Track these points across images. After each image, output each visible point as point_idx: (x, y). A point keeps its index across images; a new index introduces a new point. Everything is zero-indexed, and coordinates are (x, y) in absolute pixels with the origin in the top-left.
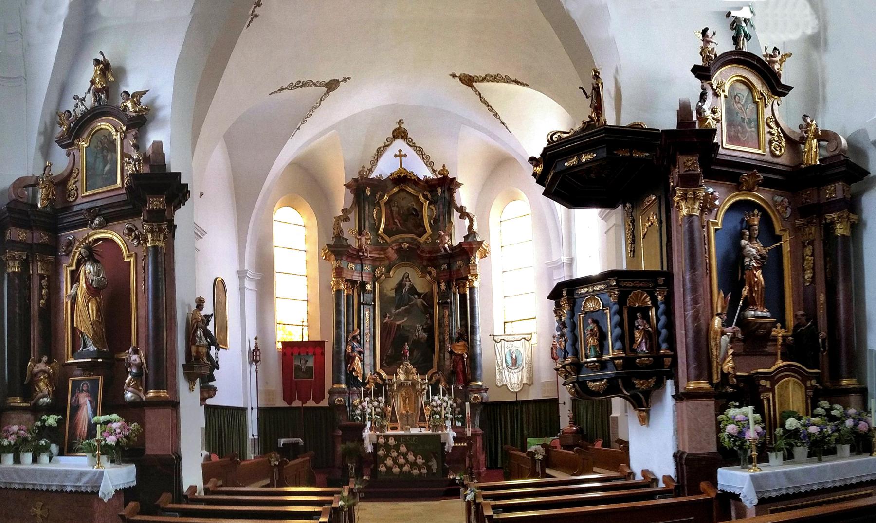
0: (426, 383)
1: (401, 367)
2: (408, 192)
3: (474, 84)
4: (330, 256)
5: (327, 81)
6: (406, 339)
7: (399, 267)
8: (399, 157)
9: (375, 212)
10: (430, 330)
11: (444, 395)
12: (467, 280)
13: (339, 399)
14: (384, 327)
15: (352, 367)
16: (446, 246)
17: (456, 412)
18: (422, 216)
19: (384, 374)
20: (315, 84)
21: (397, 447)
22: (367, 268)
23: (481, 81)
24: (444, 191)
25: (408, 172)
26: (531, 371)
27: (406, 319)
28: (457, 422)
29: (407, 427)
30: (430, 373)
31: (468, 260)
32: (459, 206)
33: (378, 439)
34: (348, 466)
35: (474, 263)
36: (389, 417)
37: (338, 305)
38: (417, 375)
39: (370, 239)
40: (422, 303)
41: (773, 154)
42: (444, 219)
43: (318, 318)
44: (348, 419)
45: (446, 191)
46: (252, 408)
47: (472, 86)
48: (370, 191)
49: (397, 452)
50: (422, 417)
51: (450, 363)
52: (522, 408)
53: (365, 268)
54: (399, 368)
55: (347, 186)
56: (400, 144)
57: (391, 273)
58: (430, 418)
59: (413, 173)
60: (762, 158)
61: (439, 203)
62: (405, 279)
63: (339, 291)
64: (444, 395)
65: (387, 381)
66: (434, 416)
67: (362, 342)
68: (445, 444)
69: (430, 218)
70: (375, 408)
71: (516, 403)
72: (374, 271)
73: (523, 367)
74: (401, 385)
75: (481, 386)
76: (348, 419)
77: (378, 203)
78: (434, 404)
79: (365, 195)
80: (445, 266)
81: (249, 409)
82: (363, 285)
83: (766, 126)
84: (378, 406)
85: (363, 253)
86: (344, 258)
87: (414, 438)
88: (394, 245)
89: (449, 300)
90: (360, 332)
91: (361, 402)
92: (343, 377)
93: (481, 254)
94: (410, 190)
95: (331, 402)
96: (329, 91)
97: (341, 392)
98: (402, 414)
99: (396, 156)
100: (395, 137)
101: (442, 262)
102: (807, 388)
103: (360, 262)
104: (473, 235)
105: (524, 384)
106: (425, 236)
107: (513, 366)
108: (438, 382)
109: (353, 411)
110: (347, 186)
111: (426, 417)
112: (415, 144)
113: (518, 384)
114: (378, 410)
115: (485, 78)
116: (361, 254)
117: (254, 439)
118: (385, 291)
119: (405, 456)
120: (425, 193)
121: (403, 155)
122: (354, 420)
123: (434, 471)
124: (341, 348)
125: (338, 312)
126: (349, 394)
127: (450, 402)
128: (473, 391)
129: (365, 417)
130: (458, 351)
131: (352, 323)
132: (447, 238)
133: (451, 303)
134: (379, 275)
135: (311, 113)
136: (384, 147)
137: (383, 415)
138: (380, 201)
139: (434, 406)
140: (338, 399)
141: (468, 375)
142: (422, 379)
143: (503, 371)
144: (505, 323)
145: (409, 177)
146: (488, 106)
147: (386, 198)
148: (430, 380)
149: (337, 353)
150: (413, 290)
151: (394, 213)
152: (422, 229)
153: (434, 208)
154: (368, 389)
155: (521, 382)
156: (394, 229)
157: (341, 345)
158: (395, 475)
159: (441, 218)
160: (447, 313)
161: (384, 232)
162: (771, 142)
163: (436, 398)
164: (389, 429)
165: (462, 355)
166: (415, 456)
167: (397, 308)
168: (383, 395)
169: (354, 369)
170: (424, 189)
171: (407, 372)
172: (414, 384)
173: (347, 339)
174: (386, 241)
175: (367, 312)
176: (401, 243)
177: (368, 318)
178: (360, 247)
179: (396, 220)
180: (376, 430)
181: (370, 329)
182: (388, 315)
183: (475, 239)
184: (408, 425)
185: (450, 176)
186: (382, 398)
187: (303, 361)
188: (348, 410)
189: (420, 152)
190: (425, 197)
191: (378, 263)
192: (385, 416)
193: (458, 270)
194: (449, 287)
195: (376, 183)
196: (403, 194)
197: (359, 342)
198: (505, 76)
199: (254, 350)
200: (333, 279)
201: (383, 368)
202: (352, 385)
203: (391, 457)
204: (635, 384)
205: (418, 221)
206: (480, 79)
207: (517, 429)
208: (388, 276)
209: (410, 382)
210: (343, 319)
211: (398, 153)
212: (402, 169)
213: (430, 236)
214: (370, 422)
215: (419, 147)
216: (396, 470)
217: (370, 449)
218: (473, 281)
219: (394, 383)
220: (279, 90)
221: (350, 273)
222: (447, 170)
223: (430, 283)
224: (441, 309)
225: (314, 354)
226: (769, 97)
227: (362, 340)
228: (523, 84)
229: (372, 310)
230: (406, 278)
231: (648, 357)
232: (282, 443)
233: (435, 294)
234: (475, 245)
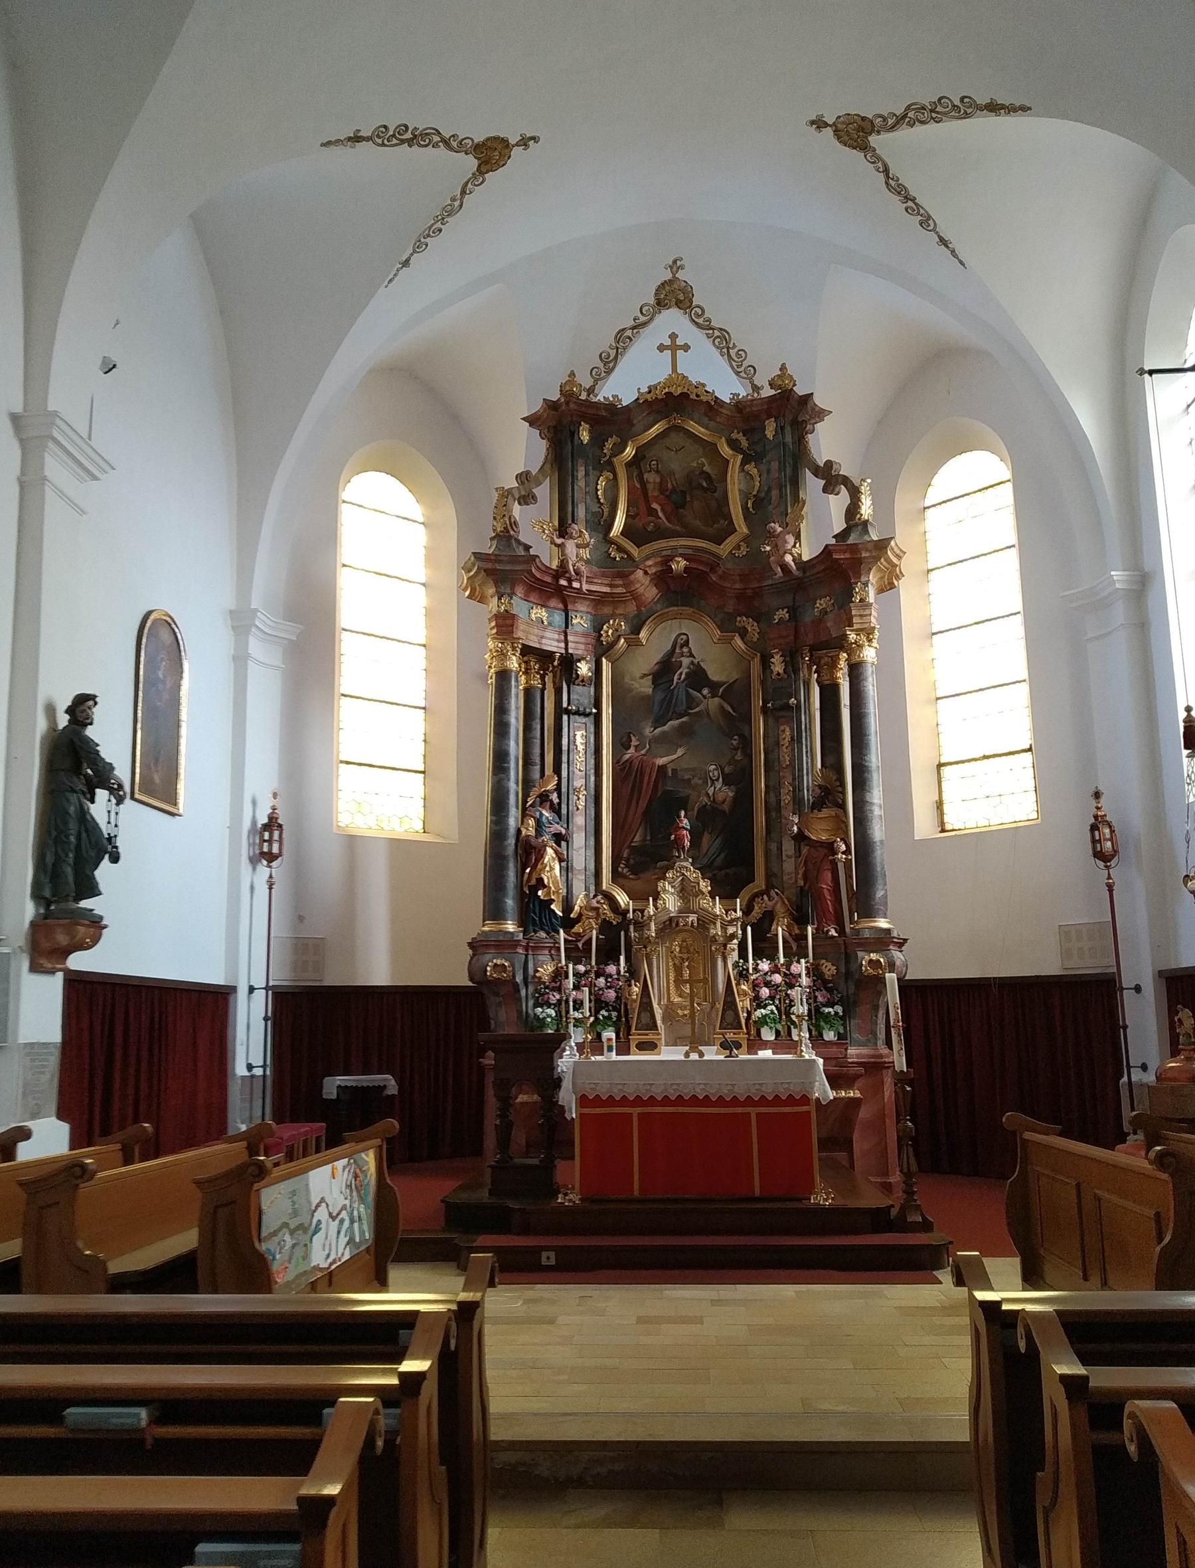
1: (669, 875)
3: (873, 140)
5: (479, 138)
6: (683, 803)
7: (662, 618)
9: (602, 483)
10: (741, 779)
12: (842, 648)
13: (499, 962)
14: (622, 772)
15: (534, 876)
18: (726, 492)
19: (622, 899)
20: (446, 143)
22: (581, 622)
23: (893, 128)
24: (782, 428)
25: (691, 384)
27: (680, 752)
30: (747, 892)
31: (849, 594)
37: (501, 710)
38: (713, 898)
39: (587, 545)
43: (58, 346)
45: (788, 429)
46: (252, 989)
47: (864, 147)
48: (590, 432)
54: (664, 878)
55: (532, 420)
56: (672, 320)
57: (643, 634)
59: (704, 385)
63: (503, 676)
65: (630, 915)
67: (564, 811)
69: (745, 496)
72: (598, 629)
74: (669, 926)
80: (783, 614)
82: (569, 662)
85: (570, 581)
86: (520, 591)
88: (650, 563)
90: (559, 785)
92: (510, 903)
96: (483, 169)
97: (505, 944)
99: (661, 348)
100: (661, 304)
103: (561, 606)
108: (769, 917)
110: (532, 420)
112: (709, 320)
115: (905, 116)
116: (563, 582)
117: (252, 1077)
120: (734, 436)
125: (501, 729)
126: (526, 948)
130: (820, 833)
131: (538, 760)
132: (791, 539)
133: (798, 706)
135: (439, 225)
136: (633, 328)
145: (693, 397)
146: (907, 198)
147: (629, 451)
148: (747, 911)
150: (698, 677)
151: (650, 487)
152: (724, 523)
153: (754, 472)
157: (507, 816)
159: (775, 493)
167: (659, 722)
169: (540, 883)
171: (686, 891)
173: (525, 802)
175: (579, 734)
176: (671, 558)
177: (581, 748)
179: (655, 506)
181: (586, 777)
182: (634, 742)
185: (800, 390)
188: (523, 992)
189: (722, 340)
191: (607, 610)
193: (819, 621)
194: (792, 665)
196: (675, 439)
197: (556, 810)
198: (962, 99)
200: (491, 644)
201: (620, 880)
202: (534, 923)
208: (633, 643)
209: (692, 918)
210: (515, 748)
211: (668, 342)
212: (677, 377)
213: (745, 539)
218: (860, 647)
219: (650, 918)
220: (350, 139)
221: (536, 631)
223: (743, 662)
224: (771, 721)
227: (564, 806)
228: (1011, 109)
230: (682, 647)
233: (756, 685)
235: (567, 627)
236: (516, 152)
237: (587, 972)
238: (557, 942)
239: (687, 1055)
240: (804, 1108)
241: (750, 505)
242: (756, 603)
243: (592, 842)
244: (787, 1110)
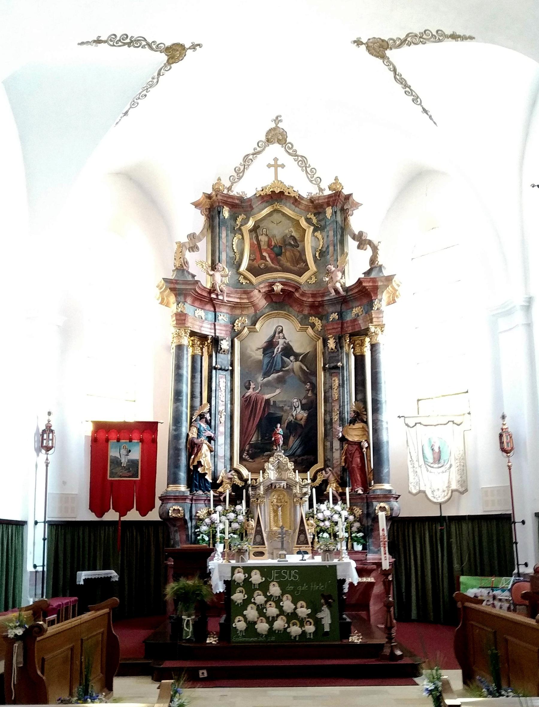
0: (308, 484)
1: (271, 459)
2: (284, 214)
3: (388, 53)
4: (168, 296)
6: (279, 420)
7: (269, 316)
8: (273, 168)
9: (235, 240)
11: (335, 502)
12: (366, 335)
13: (176, 508)
16: (338, 285)
17: (354, 529)
18: (304, 247)
19: (245, 472)
21: (264, 587)
22: (223, 318)
23: (399, 46)
24: (336, 212)
26: (463, 471)
27: (278, 391)
28: (355, 544)
29: (281, 552)
31: (371, 305)
32: (357, 233)
33: (233, 574)
34: (182, 620)
35: (378, 309)
36: (252, 537)
37: (178, 367)
38: (295, 472)
40: (301, 368)
44: (188, 539)
45: (339, 213)
46: (36, 523)
47: (383, 57)
49: (265, 595)
50: (302, 535)
51: (341, 457)
52: (450, 527)
53: (220, 318)
54: (268, 461)
56: (275, 150)
57: (258, 326)
58: (314, 539)
61: (328, 228)
62: (277, 335)
63: (180, 348)
64: (335, 502)
66: (320, 535)
68: (344, 581)
69: (315, 250)
70: (230, 523)
71: (440, 519)
72: (233, 323)
73: (451, 466)
74: (271, 488)
75: (390, 491)
76: (188, 539)
77: (240, 229)
78: (320, 516)
79: (221, 217)
80: (335, 316)
81: (31, 524)
82: (216, 341)
84: (236, 520)
85: (217, 295)
87: (293, 572)
88: (262, 286)
89: (339, 364)
91: (209, 514)
92: (183, 475)
93: (389, 297)
94: (287, 211)
95: (164, 515)
97: (179, 498)
98: (271, 531)
99: (269, 166)
100: (269, 141)
103: (212, 309)
104: (378, 269)
105: (452, 491)
106: (307, 275)
107: (434, 462)
108: (326, 482)
109: (197, 527)
111: (309, 536)
112: (296, 151)
113: (444, 491)
114: (235, 526)
115: (406, 40)
116: (213, 296)
117: (36, 572)
118: (249, 351)
119: (278, 601)
120: (309, 216)
121: (280, 166)
122: (196, 542)
123: (327, 629)
124: (181, 431)
125: (178, 378)
126: (192, 500)
127: (345, 513)
128: (378, 498)
129: (214, 536)
133: (343, 367)
134: (240, 328)
136: (253, 154)
137: (242, 534)
138: (242, 228)
139: (319, 520)
140: (172, 508)
141: (369, 473)
142: (303, 479)
143: (418, 470)
144: (418, 400)
147: (251, 224)
148: (314, 479)
149: (175, 437)
150: (288, 351)
151: (262, 244)
153: (320, 237)
154: (221, 493)
155: (448, 487)
157: (181, 426)
158: (259, 635)
159: (331, 248)
160: (337, 382)
161: (247, 269)
163: (323, 507)
164: (251, 553)
165: (359, 444)
166: (295, 602)
167: (266, 374)
168: (244, 502)
169: (199, 463)
170: (308, 210)
171: (280, 468)
172: (289, 487)
173: (191, 419)
174: (251, 282)
178: (213, 286)
179: (265, 254)
180: (231, 557)
182: (252, 386)
183: (381, 275)
184: (282, 548)
186: (242, 508)
187: (123, 452)
188: (189, 525)
189: (303, 162)
190: (308, 220)
191: (238, 312)
192: (246, 534)
195: (237, 202)
196: (276, 217)
197: (209, 423)
199: (44, 432)
201: (245, 463)
203: (255, 603)
205: (298, 254)
206: (398, 43)
207: (442, 562)
208: (252, 331)
209: (284, 484)
210: (186, 389)
213: (314, 274)
214: (222, 545)
215: (302, 156)
216: (262, 627)
217: (220, 588)
221: (198, 323)
222: (340, 184)
223: (314, 341)
224: (328, 375)
225: (142, 441)
229: (229, 378)
230: (279, 333)
232: (83, 578)
234: (382, 281)
235: (215, 321)
241: (317, 255)
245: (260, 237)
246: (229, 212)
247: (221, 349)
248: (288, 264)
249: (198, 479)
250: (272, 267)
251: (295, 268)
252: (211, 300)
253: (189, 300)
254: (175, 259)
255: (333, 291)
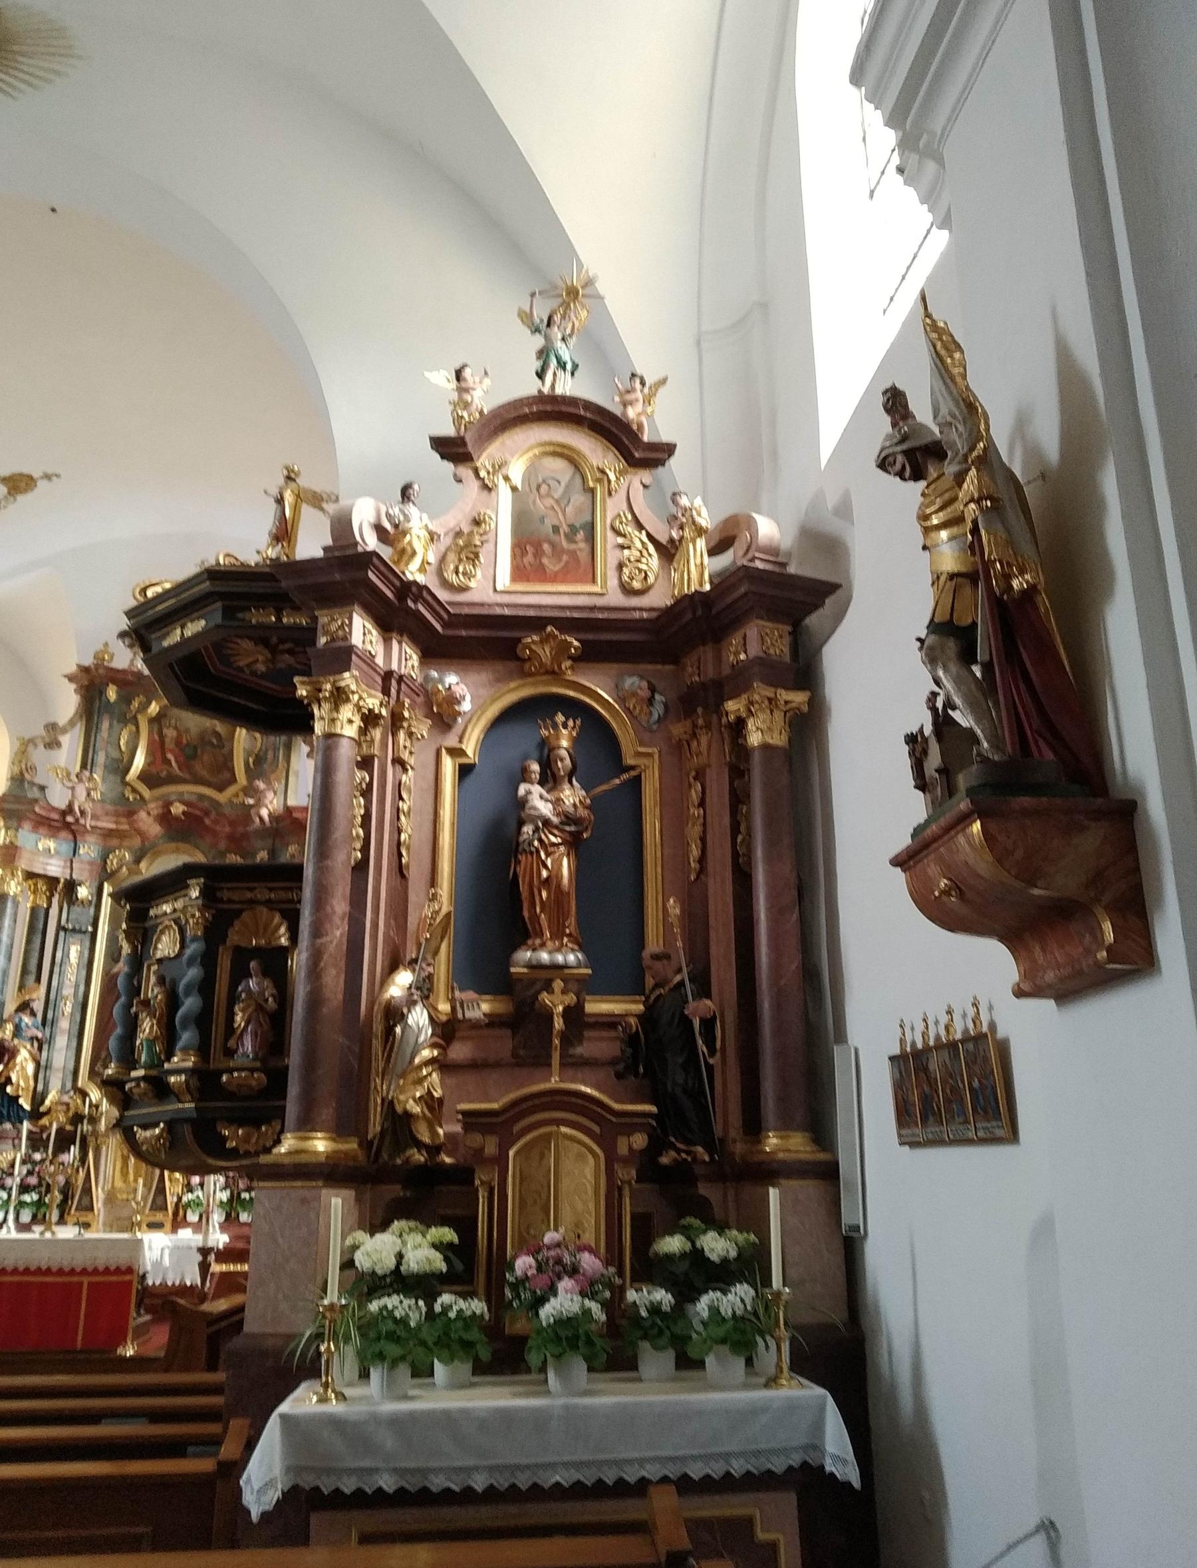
41: (627, 590)
42: (276, 757)
53: (81, 851)
60: (600, 602)
69: (248, 753)
72: (104, 860)
77: (135, 718)
83: (610, 534)
101: (258, 843)
102: (611, 1159)
116: (70, 819)
151: (167, 740)
152: (227, 775)
154: (44, 1129)
156: (164, 774)
159: (270, 755)
162: (620, 566)
174: (141, 796)
179: (170, 756)
181: (77, 986)
186: (72, 1155)
191: (115, 842)
195: (130, 678)
204: (224, 1139)
226: (622, 473)
229: (87, 944)
231: (252, 1070)
235: (74, 855)
236: (42, 485)
237: (43, 1161)
238: (19, 1132)
239: (42, 1233)
240: (127, 1278)
241: (251, 760)
242: (244, 844)
243: (74, 1044)
244: (114, 1278)
245: (165, 731)
246: (117, 692)
247: (77, 899)
248: (204, 773)
249: (6, 1104)
250: (177, 776)
251: (214, 780)
252: (67, 826)
253: (27, 826)
254: (13, 763)
255: (257, 820)
